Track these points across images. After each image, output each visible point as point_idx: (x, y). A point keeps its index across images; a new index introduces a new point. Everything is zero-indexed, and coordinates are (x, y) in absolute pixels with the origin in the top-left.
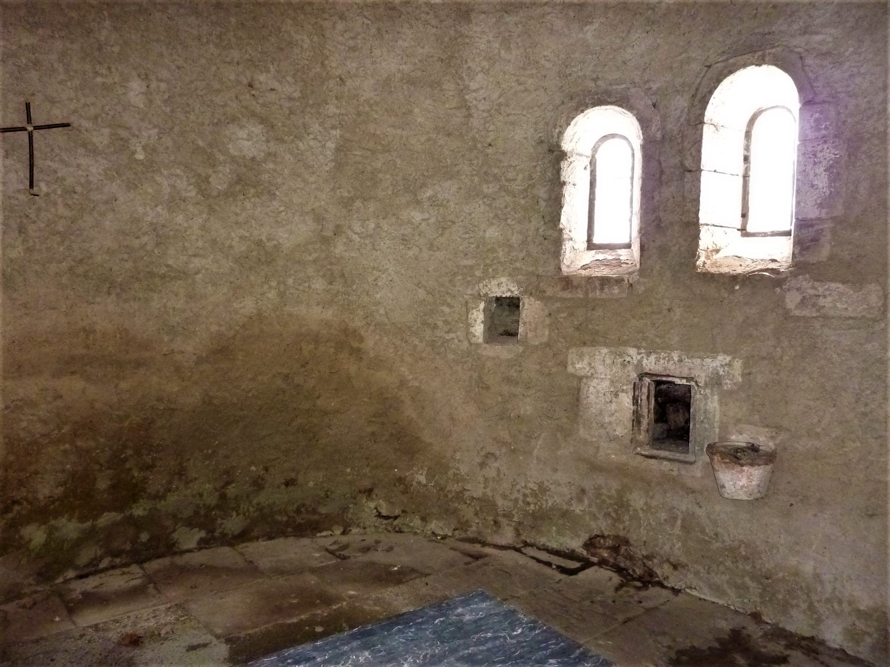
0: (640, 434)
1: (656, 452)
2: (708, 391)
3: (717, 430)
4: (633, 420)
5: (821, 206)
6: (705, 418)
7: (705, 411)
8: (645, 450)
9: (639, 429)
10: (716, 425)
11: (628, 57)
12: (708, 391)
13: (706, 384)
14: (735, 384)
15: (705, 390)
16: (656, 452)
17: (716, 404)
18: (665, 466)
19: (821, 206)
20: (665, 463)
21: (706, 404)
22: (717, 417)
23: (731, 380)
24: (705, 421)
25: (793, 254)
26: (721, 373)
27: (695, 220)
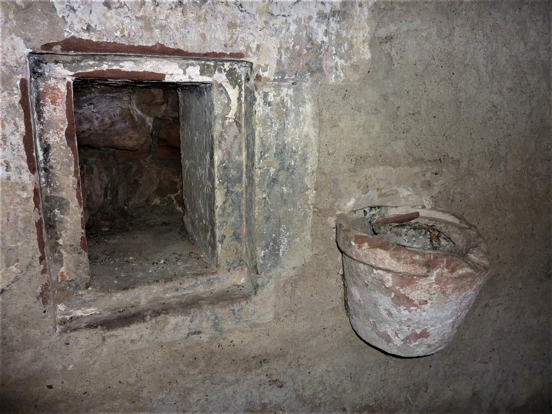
0: (59, 261)
1: (120, 299)
2: (287, 92)
3: (311, 194)
4: (39, 225)
5: (234, 88)
6: (282, 167)
7: (281, 152)
8: (85, 304)
9: (55, 247)
10: (309, 181)
11: (15, 40)
12: (287, 92)
13: (281, 73)
14: (355, 67)
15: (278, 88)
16: (120, 299)
17: (308, 129)
18: (176, 327)
19: (234, 88)
20: (173, 320)
21: (283, 129)
22: (312, 164)
23: (347, 56)
24: (282, 176)
25: (182, 172)
26: (320, 37)
27: (82, 151)
